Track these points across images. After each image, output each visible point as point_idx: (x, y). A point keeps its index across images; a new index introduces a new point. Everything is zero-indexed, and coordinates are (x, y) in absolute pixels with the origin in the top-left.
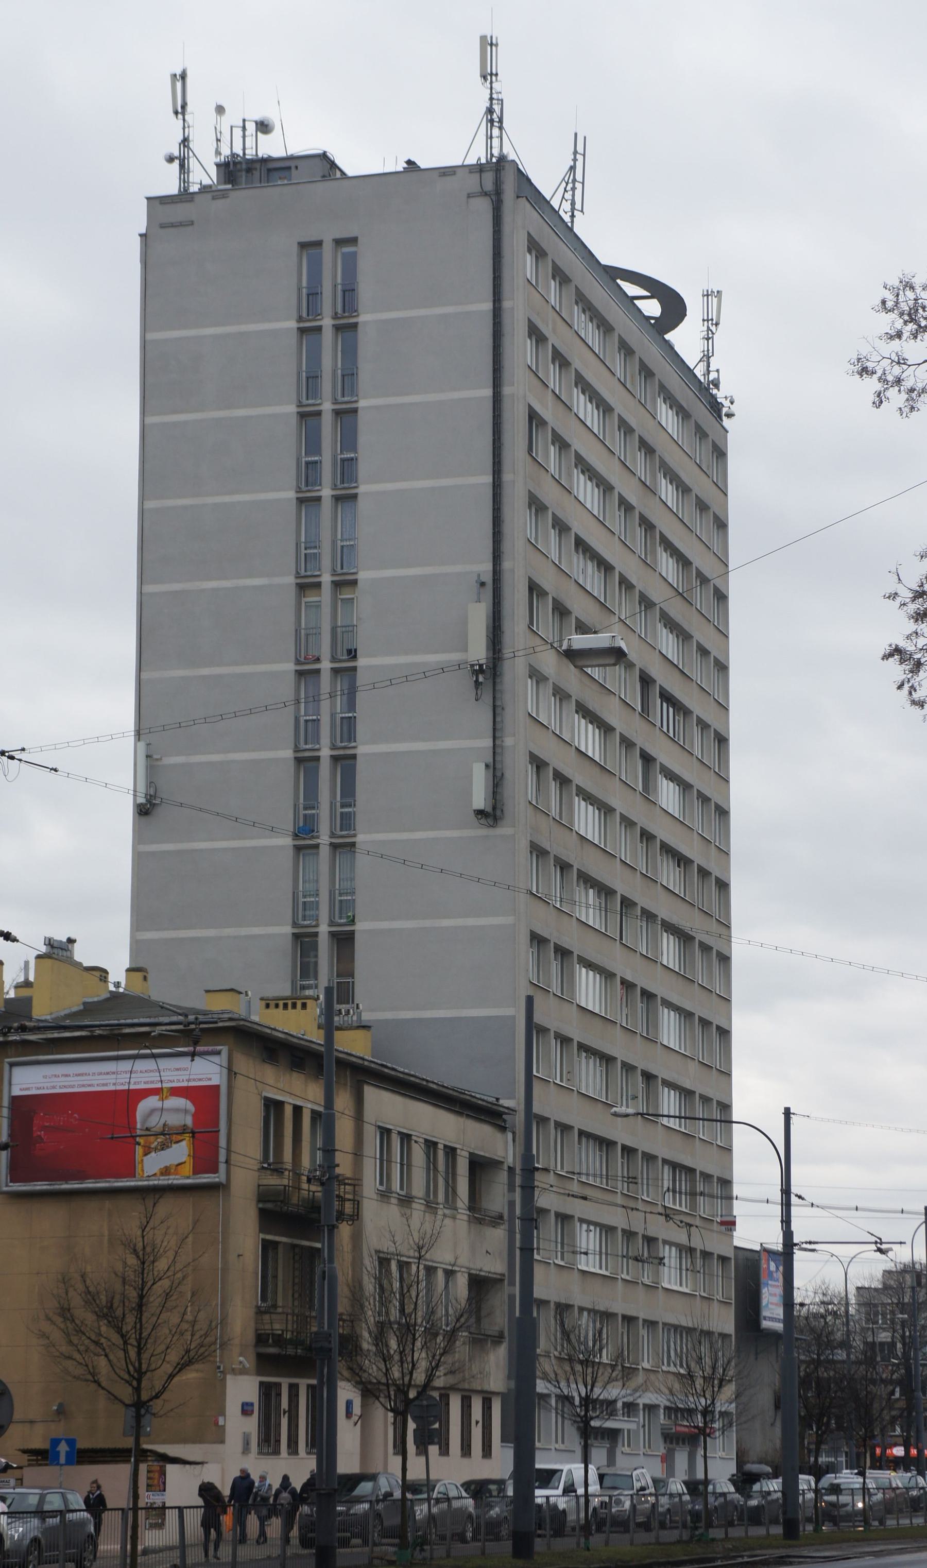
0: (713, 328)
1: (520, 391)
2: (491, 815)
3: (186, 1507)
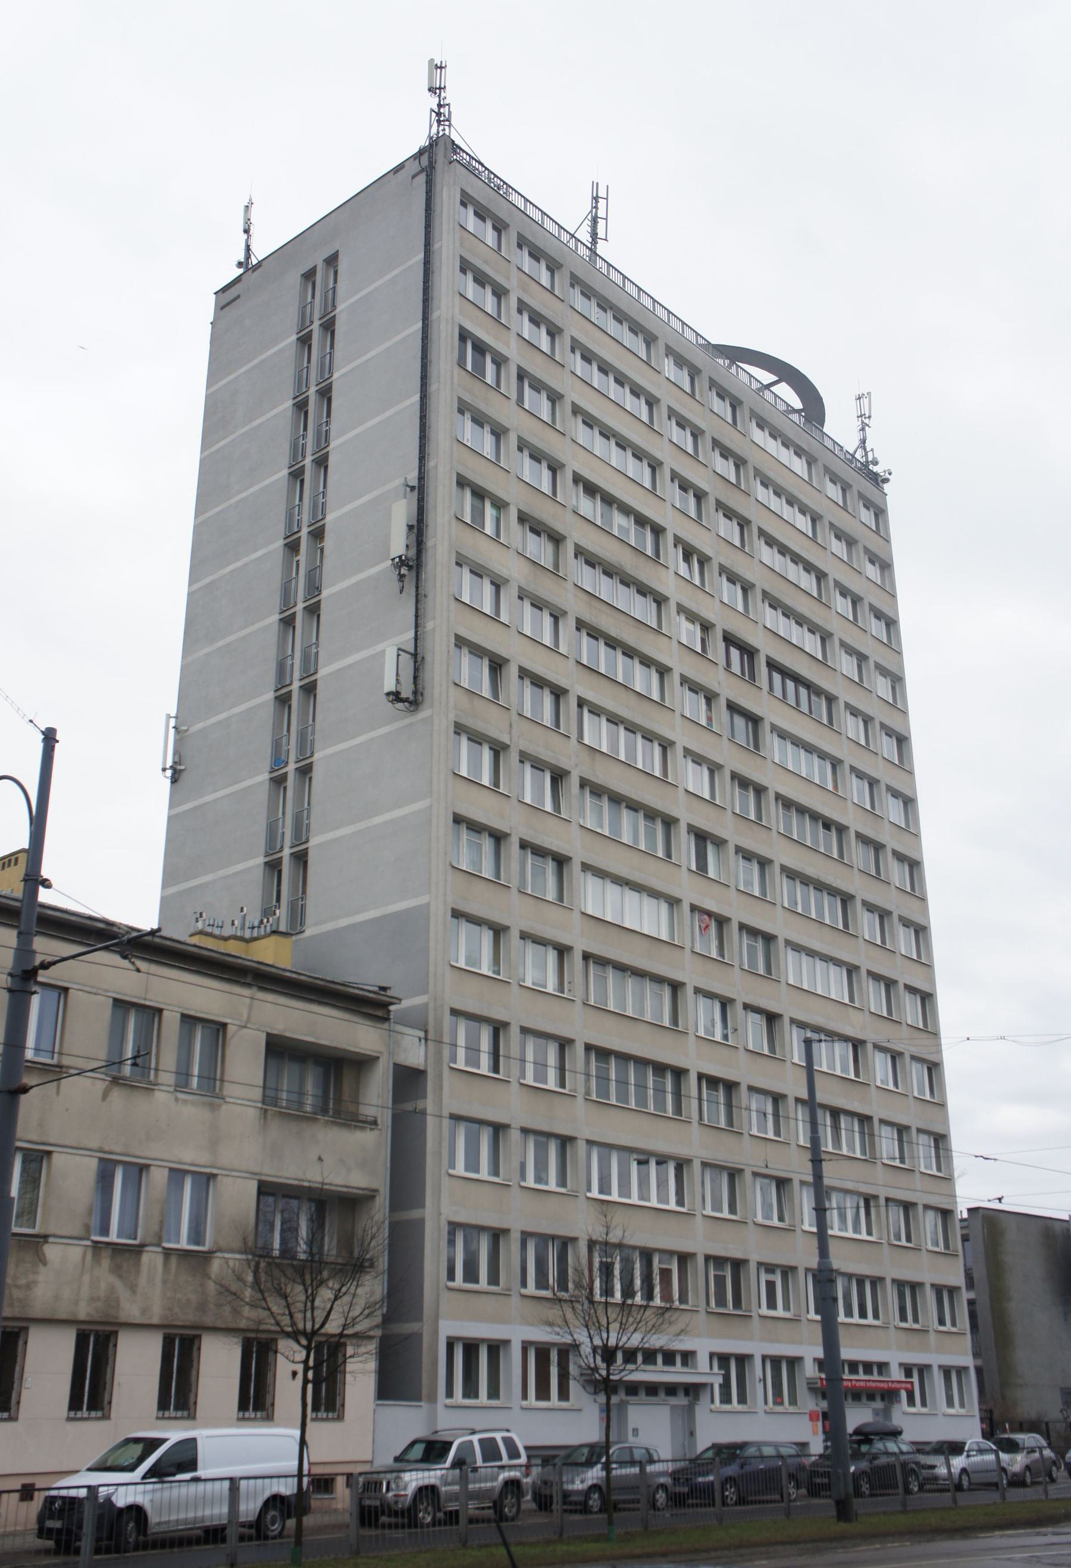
0: (867, 421)
1: (449, 314)
2: (410, 699)
3: (242, 1478)
